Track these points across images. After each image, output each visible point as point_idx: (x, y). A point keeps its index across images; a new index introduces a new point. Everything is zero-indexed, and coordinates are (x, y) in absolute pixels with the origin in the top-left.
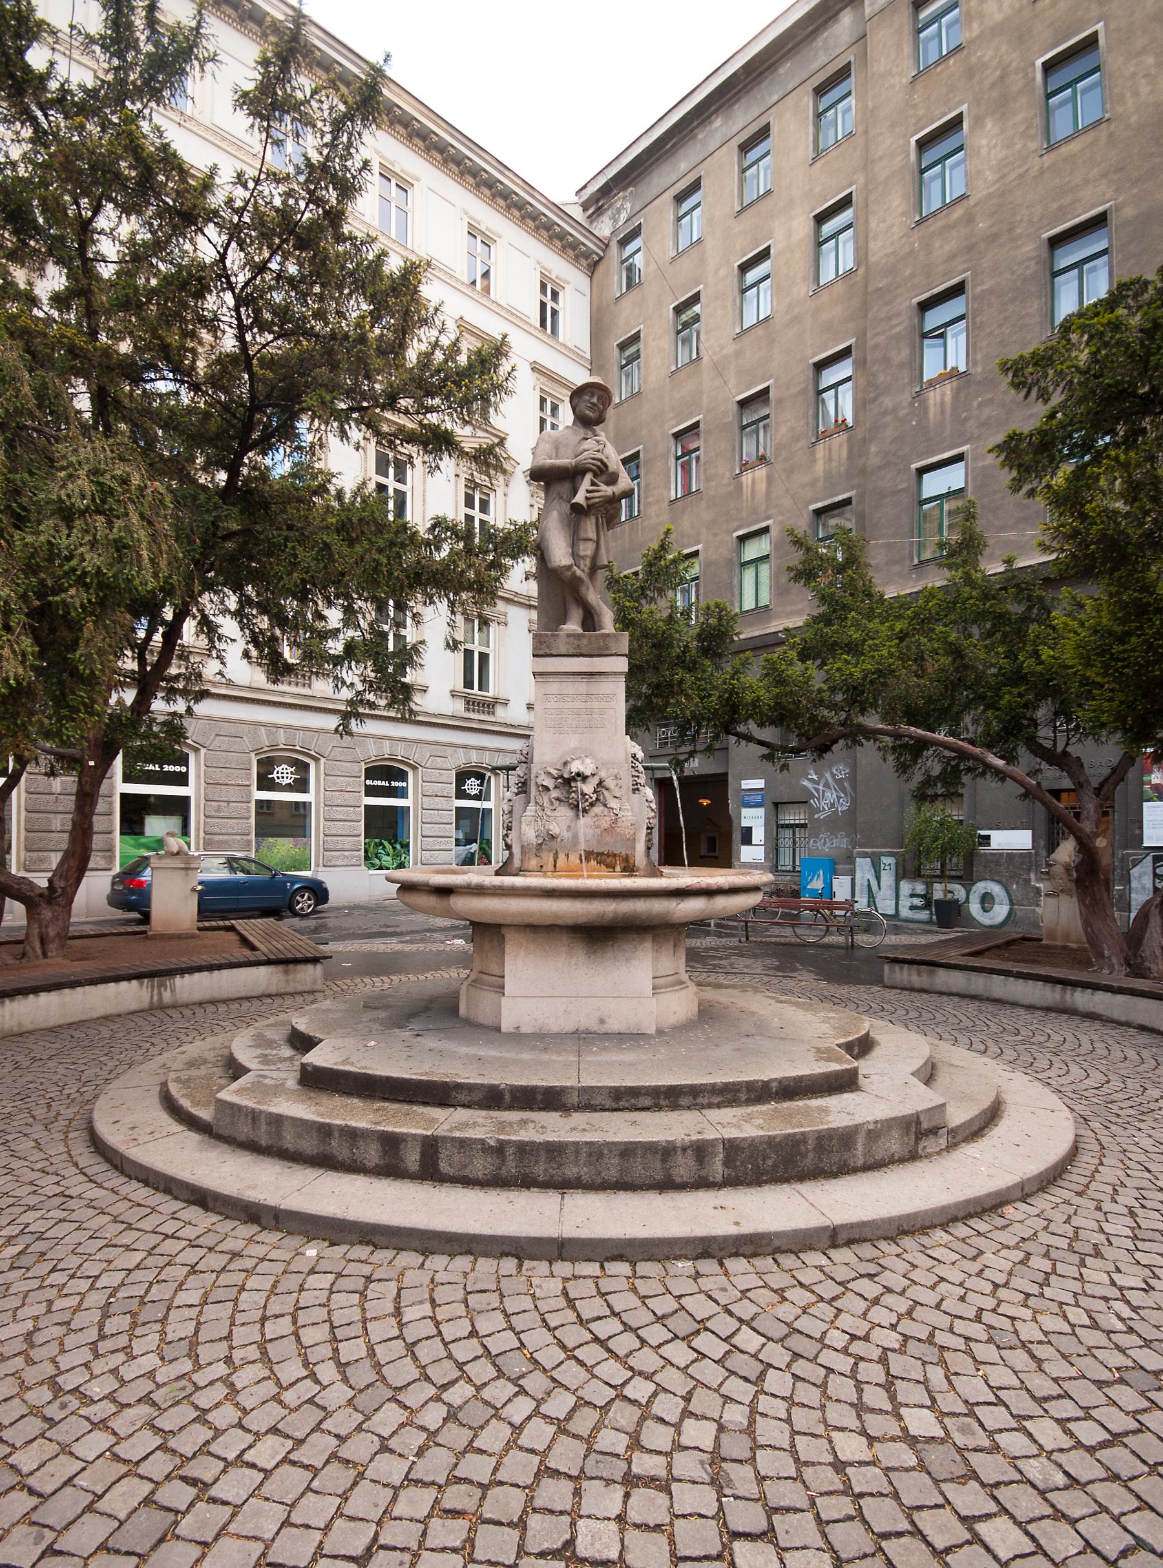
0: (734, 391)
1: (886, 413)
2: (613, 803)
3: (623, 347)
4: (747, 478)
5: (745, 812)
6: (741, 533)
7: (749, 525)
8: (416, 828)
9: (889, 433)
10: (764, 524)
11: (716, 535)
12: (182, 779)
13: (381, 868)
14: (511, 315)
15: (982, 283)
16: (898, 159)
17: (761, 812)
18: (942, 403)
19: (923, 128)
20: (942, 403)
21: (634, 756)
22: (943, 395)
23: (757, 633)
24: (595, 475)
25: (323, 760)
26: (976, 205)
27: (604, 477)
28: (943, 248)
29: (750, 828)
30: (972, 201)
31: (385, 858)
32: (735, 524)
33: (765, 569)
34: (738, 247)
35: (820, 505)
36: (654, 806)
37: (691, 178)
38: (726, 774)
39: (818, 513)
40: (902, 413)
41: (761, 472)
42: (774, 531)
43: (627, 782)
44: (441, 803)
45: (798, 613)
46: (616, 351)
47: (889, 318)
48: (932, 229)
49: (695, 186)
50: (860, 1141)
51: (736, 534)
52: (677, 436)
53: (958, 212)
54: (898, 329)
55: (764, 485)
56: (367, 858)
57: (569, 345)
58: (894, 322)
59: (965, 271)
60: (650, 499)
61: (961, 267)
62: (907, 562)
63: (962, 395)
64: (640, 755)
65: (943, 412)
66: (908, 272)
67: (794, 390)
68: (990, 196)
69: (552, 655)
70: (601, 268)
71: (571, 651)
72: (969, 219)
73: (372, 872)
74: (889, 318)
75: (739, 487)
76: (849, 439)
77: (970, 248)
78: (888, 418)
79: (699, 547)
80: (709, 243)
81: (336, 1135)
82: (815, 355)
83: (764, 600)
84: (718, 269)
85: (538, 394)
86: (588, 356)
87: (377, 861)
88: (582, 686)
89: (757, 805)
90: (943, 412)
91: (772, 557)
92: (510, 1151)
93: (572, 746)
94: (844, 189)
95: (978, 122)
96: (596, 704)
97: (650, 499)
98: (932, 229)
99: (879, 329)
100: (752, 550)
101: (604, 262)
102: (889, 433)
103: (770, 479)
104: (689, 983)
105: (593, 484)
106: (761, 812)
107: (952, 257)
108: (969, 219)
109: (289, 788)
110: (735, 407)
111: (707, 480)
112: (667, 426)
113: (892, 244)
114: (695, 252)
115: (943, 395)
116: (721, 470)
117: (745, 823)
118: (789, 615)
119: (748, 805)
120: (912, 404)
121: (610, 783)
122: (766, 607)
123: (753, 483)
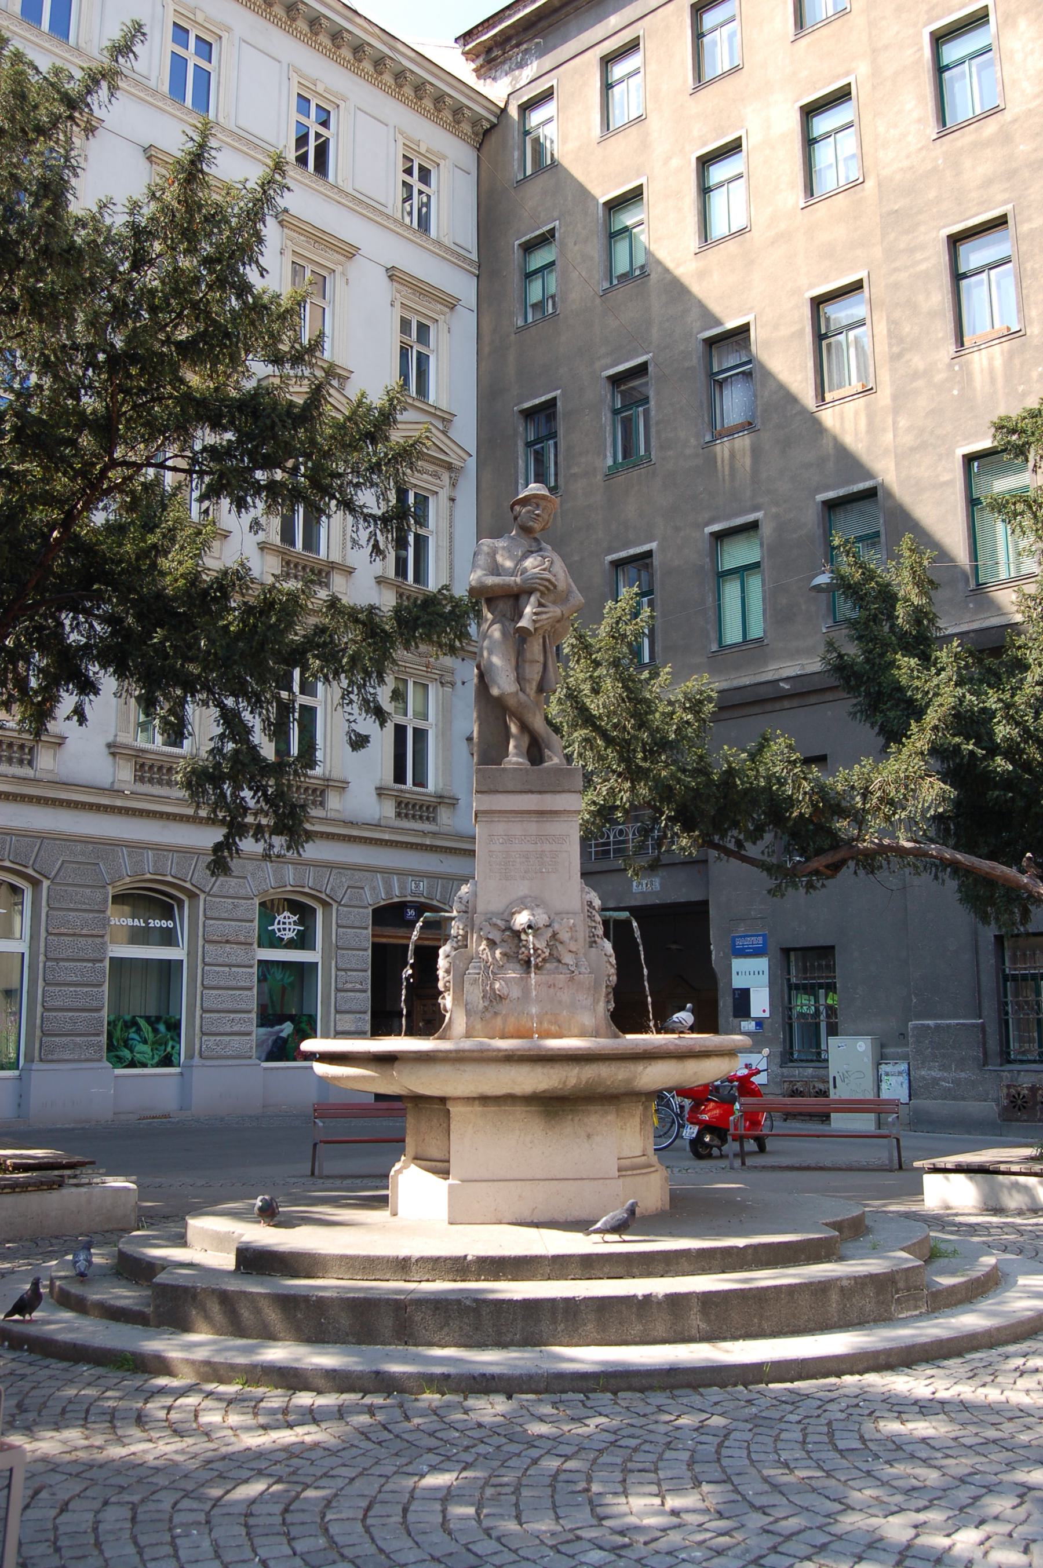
0: (698, 325)
1: (915, 375)
2: (568, 959)
3: (529, 248)
4: (722, 449)
5: (738, 964)
6: (716, 527)
7: (728, 518)
8: (192, 996)
9: (922, 403)
10: (751, 518)
11: (677, 529)
12: (168, 938)
13: (132, 1064)
14: (362, 205)
15: (1029, 220)
16: (910, 52)
17: (762, 964)
18: (991, 370)
19: (938, 18)
20: (991, 370)
21: (590, 904)
22: (991, 360)
23: (746, 681)
24: (542, 593)
25: (46, 883)
26: (1014, 121)
27: (552, 597)
28: (978, 169)
29: (748, 990)
30: (1007, 116)
31: (141, 1047)
32: (707, 515)
33: (755, 584)
34: (696, 133)
35: (831, 495)
36: (614, 962)
37: (626, 37)
38: (706, 903)
39: (831, 506)
40: (939, 378)
41: (743, 442)
42: (766, 530)
43: (582, 934)
44: (237, 954)
45: (809, 652)
46: (517, 254)
47: (911, 251)
48: (959, 144)
49: (632, 47)
50: (834, 1296)
51: (709, 529)
52: (616, 380)
53: (991, 127)
54: (923, 267)
55: (748, 461)
56: (111, 1047)
57: (446, 241)
58: (919, 256)
59: (1005, 202)
60: (575, 470)
61: (1000, 197)
62: (961, 585)
63: (1017, 362)
64: (597, 903)
65: (993, 380)
66: (932, 194)
67: (784, 331)
68: (1029, 113)
69: (498, 792)
70: (494, 138)
71: (519, 788)
72: (1005, 137)
73: (119, 1071)
74: (911, 251)
75: (711, 461)
76: (868, 406)
77: (1011, 174)
78: (920, 383)
79: (653, 546)
80: (654, 123)
81: (303, 1306)
82: (811, 286)
83: (756, 630)
84: (667, 160)
85: (398, 313)
86: (474, 257)
87: (126, 1053)
88: (533, 827)
89: (757, 953)
90: (993, 380)
91: (765, 565)
92: (485, 1311)
93: (521, 894)
94: (838, 77)
95: (1010, 19)
96: (547, 847)
97: (575, 470)
98: (959, 144)
99: (897, 264)
100: (739, 554)
101: (500, 127)
102: (922, 403)
103: (756, 451)
104: (658, 1166)
105: (541, 605)
106: (762, 964)
107: (988, 182)
108: (1005, 137)
109: (291, 944)
110: (700, 347)
111: (662, 448)
112: (598, 365)
113: (908, 157)
114: (633, 131)
115: (991, 360)
116: (682, 434)
117: (738, 983)
118: (795, 654)
119: (743, 953)
120: (950, 367)
121: (564, 936)
122: (759, 640)
123: (732, 455)
